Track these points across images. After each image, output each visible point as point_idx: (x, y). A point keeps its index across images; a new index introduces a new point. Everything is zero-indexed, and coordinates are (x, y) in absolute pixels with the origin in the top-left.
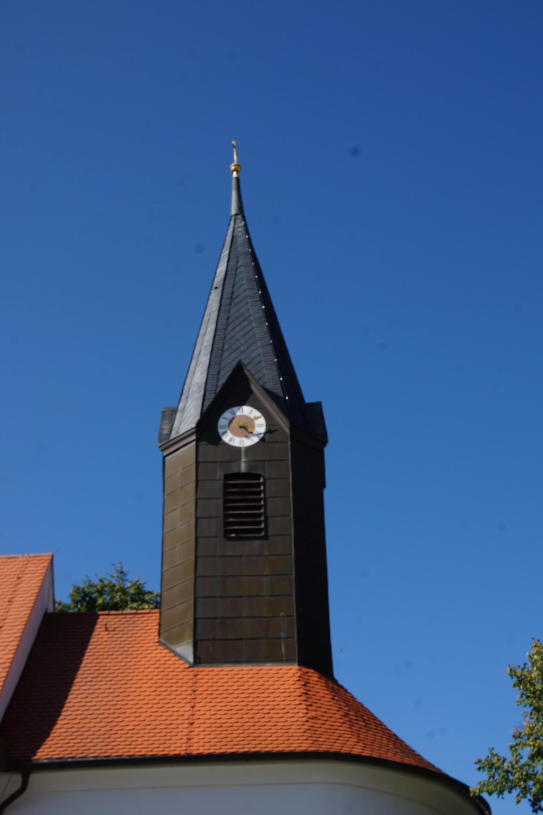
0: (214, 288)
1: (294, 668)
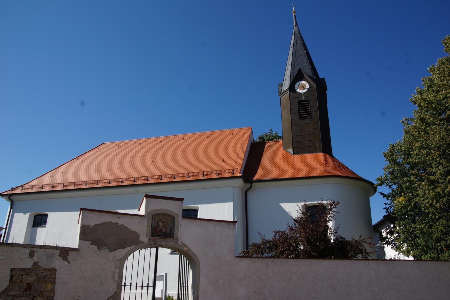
1: (322, 154)
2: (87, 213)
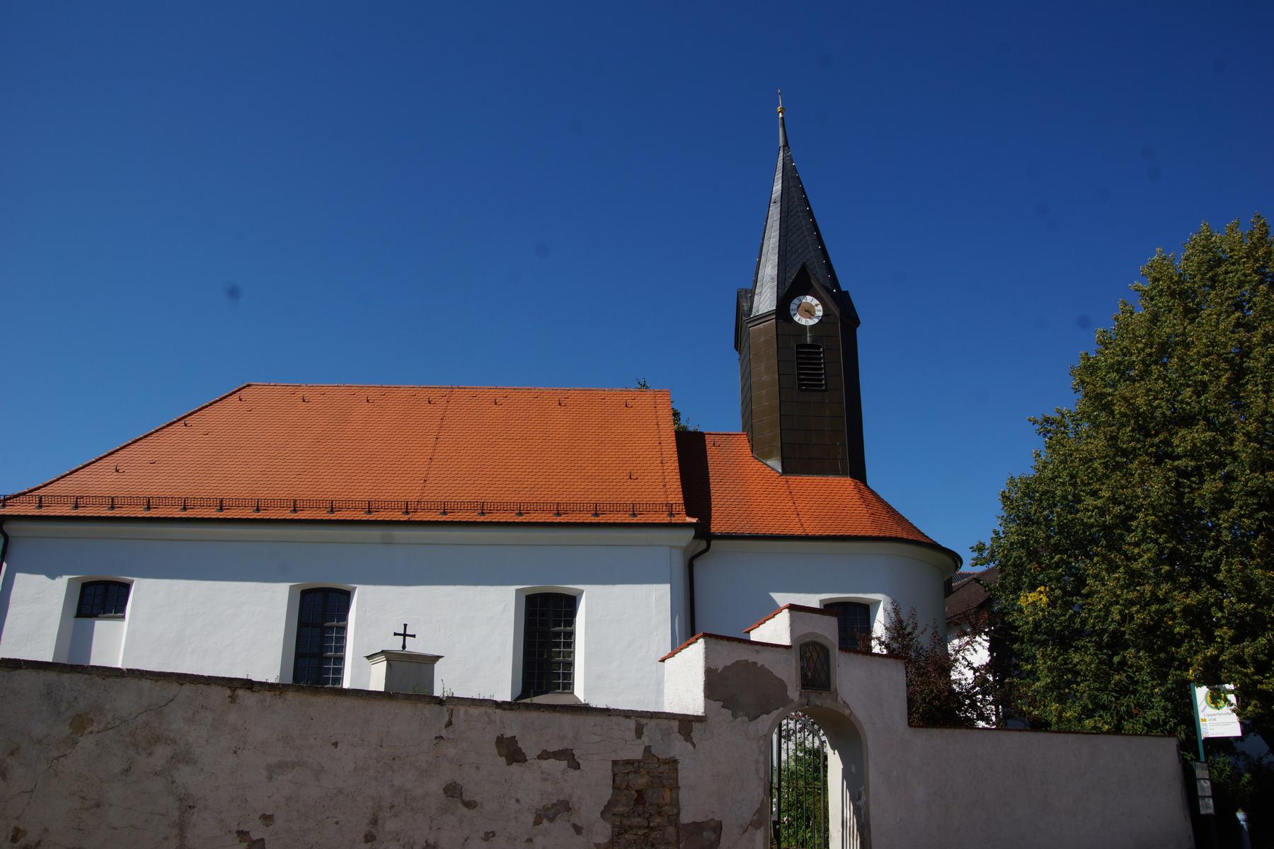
2: (713, 641)
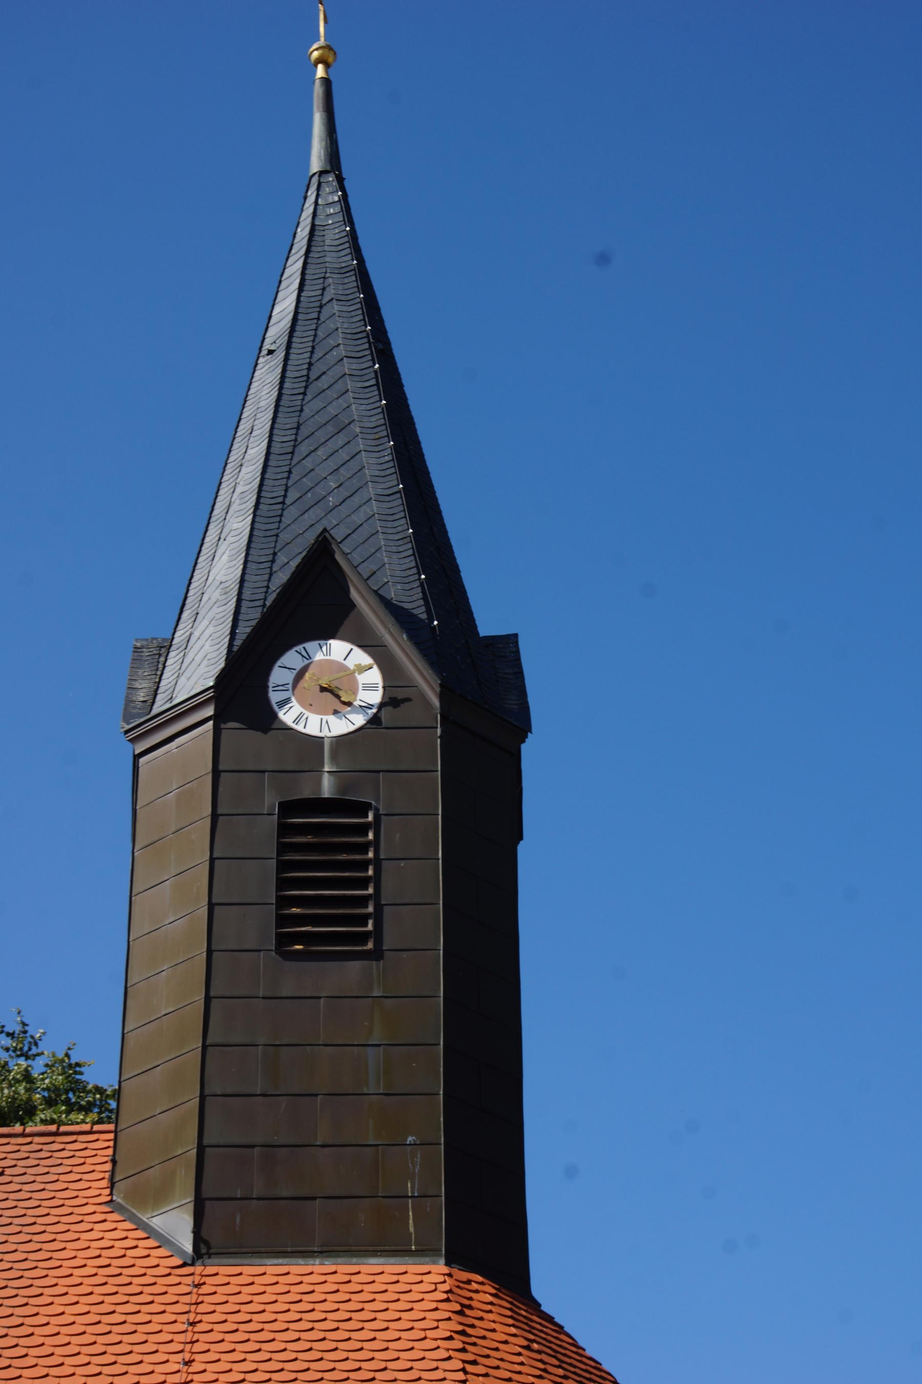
0: (264, 352)
1: (436, 1271)
